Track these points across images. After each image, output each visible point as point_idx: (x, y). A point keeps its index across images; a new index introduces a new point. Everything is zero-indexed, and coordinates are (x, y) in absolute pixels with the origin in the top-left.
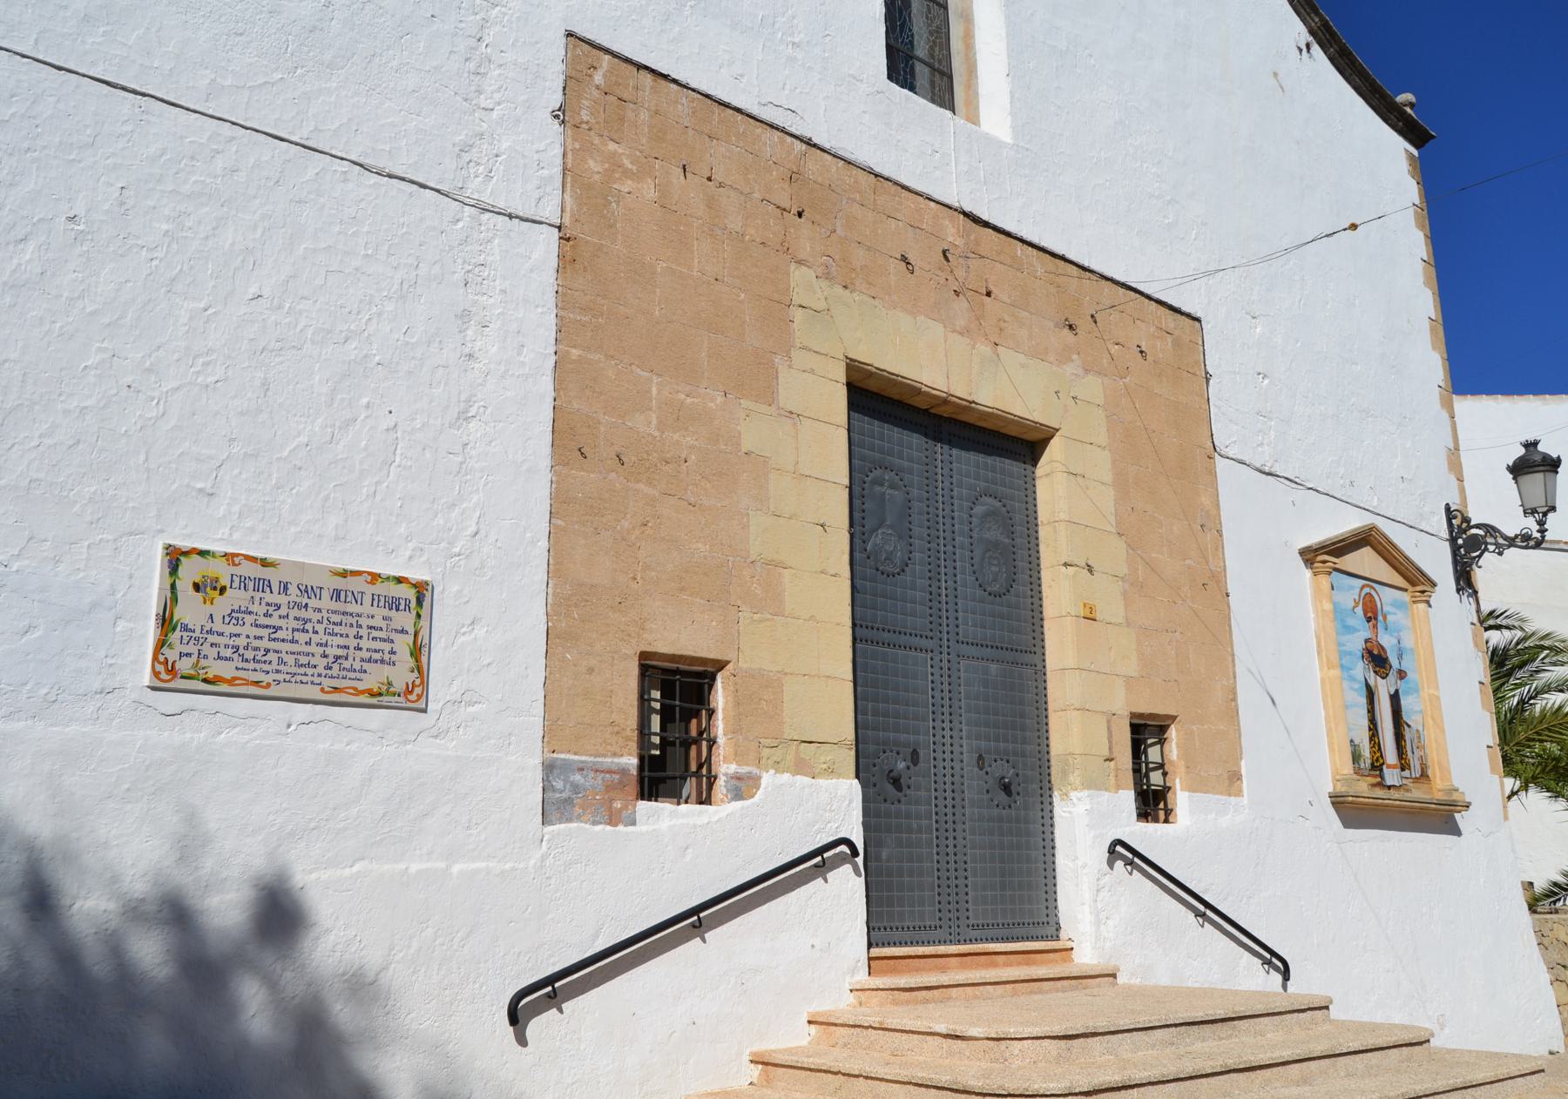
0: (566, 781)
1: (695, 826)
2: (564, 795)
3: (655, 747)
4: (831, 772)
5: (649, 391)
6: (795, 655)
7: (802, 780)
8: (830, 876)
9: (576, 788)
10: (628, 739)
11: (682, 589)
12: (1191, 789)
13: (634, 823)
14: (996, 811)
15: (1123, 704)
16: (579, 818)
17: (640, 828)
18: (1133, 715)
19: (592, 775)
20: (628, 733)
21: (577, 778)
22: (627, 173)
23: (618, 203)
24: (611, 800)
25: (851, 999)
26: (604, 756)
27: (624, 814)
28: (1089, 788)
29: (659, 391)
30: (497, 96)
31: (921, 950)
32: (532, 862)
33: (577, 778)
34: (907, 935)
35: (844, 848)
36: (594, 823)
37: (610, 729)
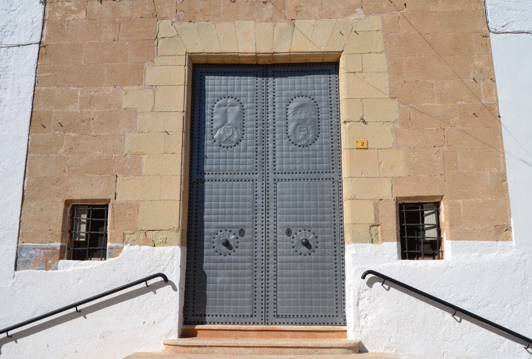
0: (27, 254)
1: (84, 270)
2: (26, 259)
3: (83, 237)
4: (165, 243)
5: (77, 95)
6: (151, 191)
7: (147, 248)
8: (158, 291)
9: (31, 256)
10: (57, 235)
11: (88, 172)
12: (454, 238)
13: (57, 269)
14: (299, 257)
15: (388, 194)
16: (32, 268)
17: (59, 271)
18: (398, 199)
19: (39, 250)
20: (57, 232)
21: (33, 252)
22: (73, 12)
23: (68, 25)
24: (47, 260)
25: (163, 347)
26: (46, 243)
27: (52, 265)
28: (355, 243)
29: (81, 94)
30: (18, 5)
31: (229, 327)
32: (9, 285)
33: (33, 252)
34: (231, 319)
35: (160, 279)
36: (38, 270)
37: (49, 232)
